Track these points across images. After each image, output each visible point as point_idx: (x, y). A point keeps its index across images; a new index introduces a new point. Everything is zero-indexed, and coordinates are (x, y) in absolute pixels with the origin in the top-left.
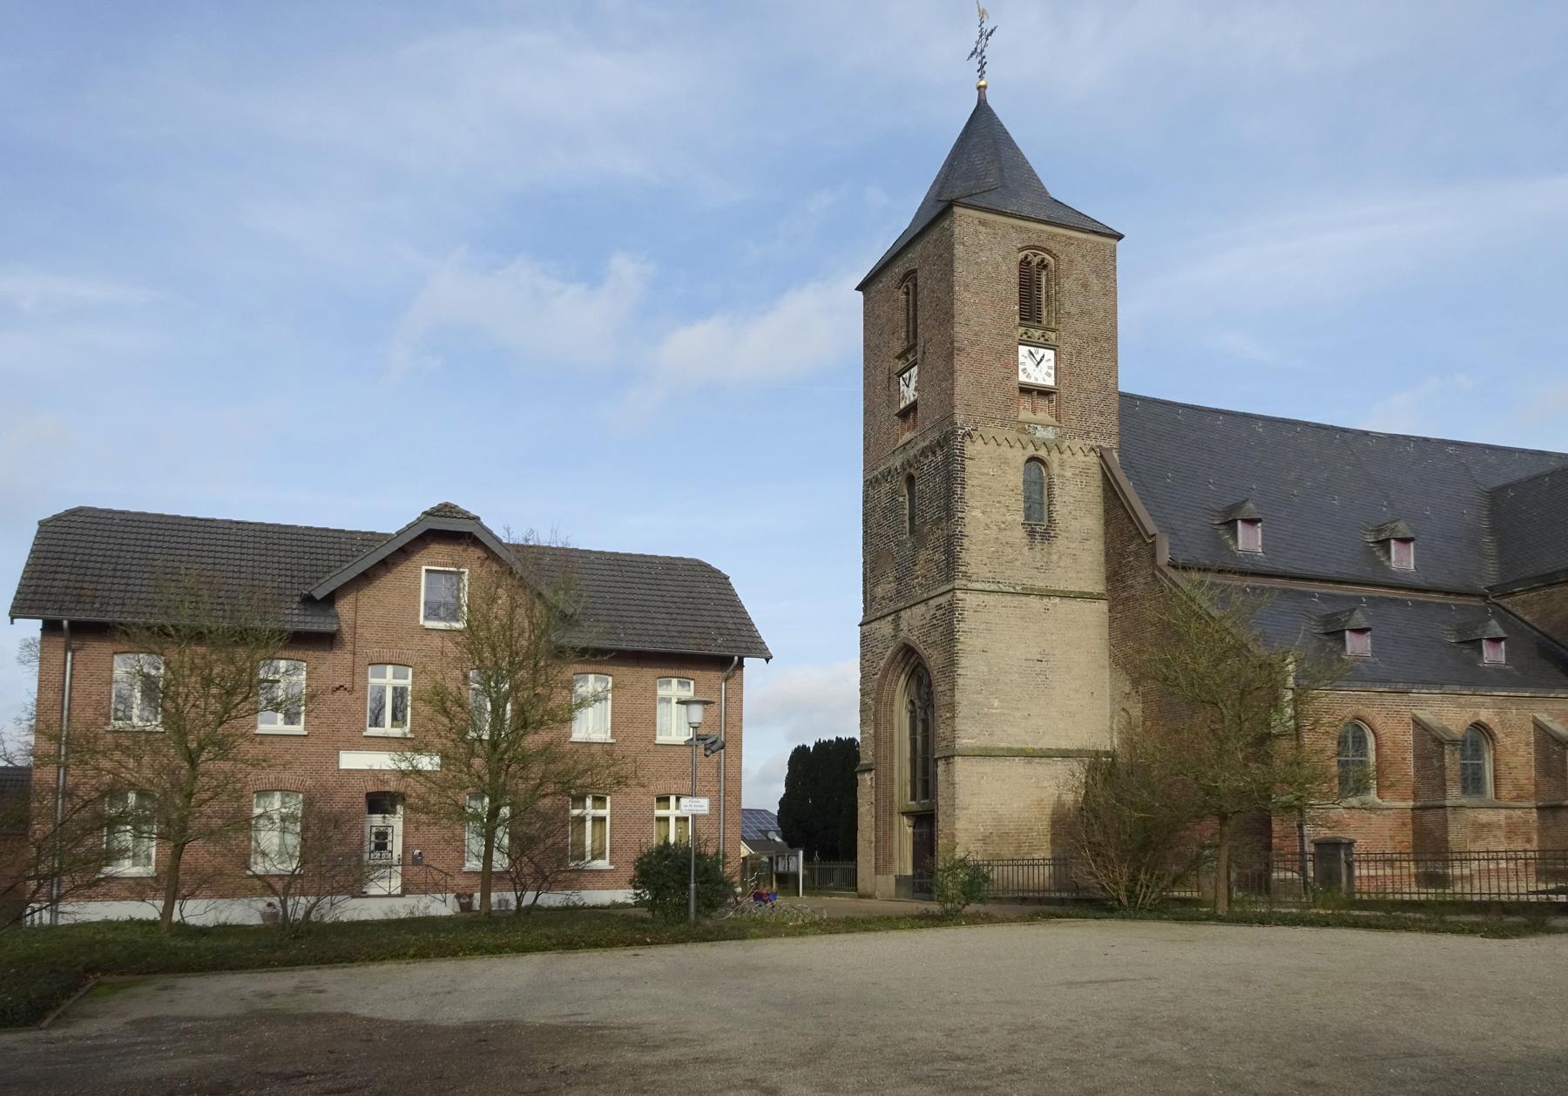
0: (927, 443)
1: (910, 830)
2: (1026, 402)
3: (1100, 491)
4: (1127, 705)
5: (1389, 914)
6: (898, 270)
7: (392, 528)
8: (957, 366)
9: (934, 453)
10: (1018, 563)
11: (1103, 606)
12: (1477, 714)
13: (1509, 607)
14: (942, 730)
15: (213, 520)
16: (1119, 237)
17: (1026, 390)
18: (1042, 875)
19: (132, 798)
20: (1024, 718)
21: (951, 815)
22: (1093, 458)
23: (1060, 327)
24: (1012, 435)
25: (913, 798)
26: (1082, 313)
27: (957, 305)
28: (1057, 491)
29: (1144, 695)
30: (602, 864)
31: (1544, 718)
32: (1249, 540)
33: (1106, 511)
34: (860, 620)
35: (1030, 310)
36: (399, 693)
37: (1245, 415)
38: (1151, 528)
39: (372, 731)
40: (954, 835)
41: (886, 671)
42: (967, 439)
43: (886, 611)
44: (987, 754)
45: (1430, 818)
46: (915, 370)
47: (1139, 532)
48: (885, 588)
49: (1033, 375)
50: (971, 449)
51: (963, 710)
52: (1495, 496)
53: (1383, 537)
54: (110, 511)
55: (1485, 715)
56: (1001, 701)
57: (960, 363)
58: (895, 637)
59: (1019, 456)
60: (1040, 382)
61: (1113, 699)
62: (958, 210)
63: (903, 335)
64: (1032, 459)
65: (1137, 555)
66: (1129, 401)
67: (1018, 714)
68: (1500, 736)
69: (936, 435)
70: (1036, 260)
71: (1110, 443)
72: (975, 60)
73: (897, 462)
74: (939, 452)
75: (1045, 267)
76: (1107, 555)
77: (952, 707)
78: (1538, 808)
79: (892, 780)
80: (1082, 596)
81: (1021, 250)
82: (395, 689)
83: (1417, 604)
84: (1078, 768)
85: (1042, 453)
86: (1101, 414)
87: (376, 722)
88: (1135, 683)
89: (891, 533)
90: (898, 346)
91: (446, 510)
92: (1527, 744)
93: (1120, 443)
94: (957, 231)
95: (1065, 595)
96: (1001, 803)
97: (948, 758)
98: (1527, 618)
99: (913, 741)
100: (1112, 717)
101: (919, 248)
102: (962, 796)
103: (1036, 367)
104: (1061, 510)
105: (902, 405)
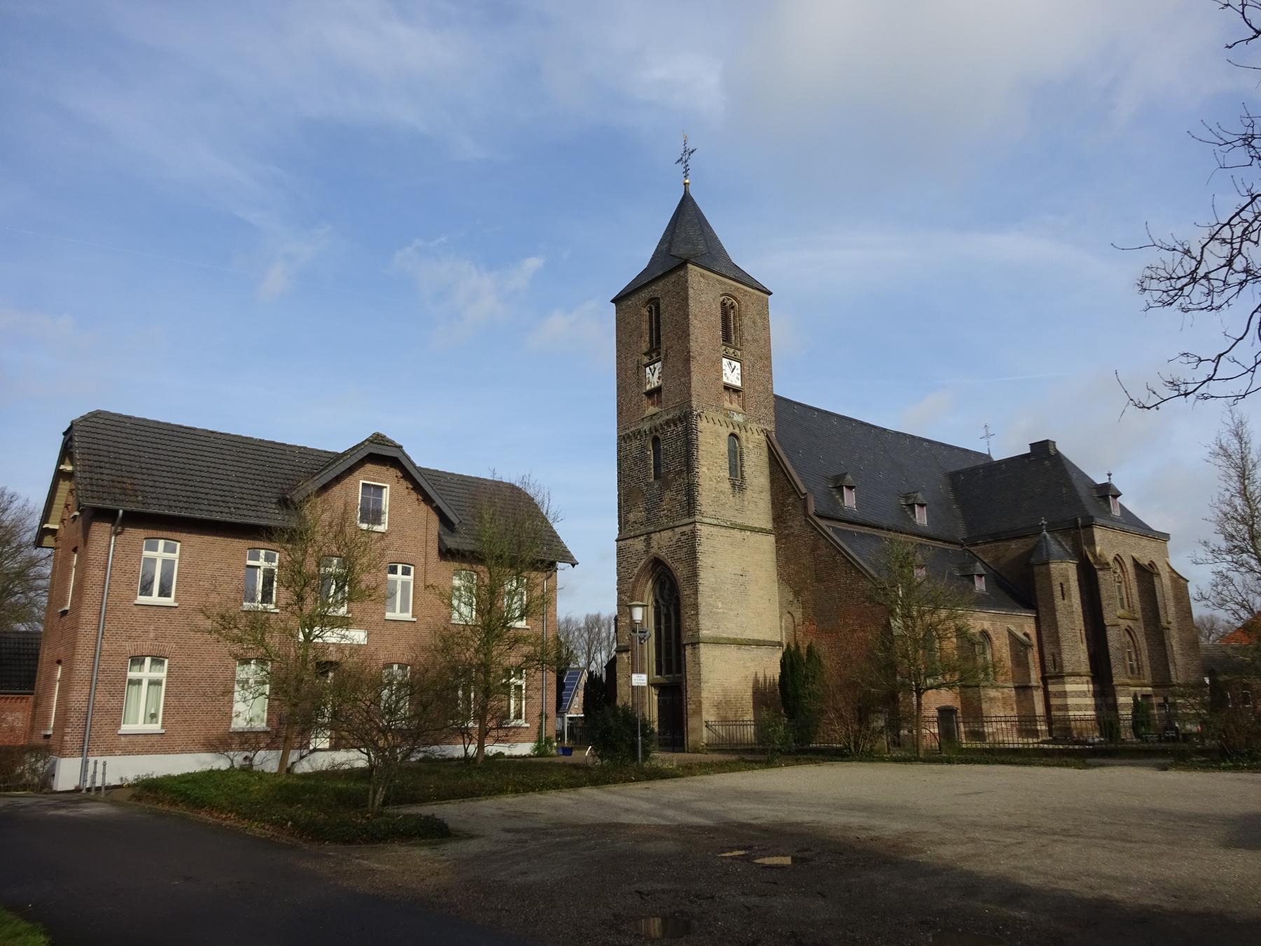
0: (670, 417)
1: (656, 698)
2: (726, 396)
4: (792, 609)
5: (932, 758)
6: (645, 295)
7: (339, 446)
9: (676, 425)
11: (772, 538)
14: (687, 623)
15: (195, 429)
16: (770, 293)
17: (727, 388)
19: (396, 667)
21: (698, 687)
22: (762, 437)
24: (722, 418)
25: (659, 673)
27: (691, 328)
30: (522, 722)
31: (1013, 628)
32: (849, 500)
35: (726, 338)
36: (168, 564)
38: (804, 491)
39: (142, 599)
40: (700, 703)
41: (638, 576)
43: (638, 532)
44: (717, 642)
45: (970, 692)
46: (658, 365)
47: (795, 491)
48: (636, 515)
50: (702, 425)
52: (953, 477)
53: (910, 502)
54: (121, 416)
55: (987, 625)
57: (694, 366)
58: (647, 552)
59: (725, 432)
61: (781, 604)
65: (794, 506)
67: (732, 613)
69: (678, 412)
72: (681, 167)
73: (646, 426)
76: (773, 503)
77: (696, 606)
80: (761, 531)
82: (164, 561)
83: (862, 535)
84: (778, 655)
85: (737, 431)
87: (146, 590)
89: (641, 476)
90: (645, 346)
91: (378, 439)
96: (729, 674)
97: (695, 644)
99: (658, 631)
100: (781, 617)
102: (705, 674)
103: (732, 374)
105: (648, 387)
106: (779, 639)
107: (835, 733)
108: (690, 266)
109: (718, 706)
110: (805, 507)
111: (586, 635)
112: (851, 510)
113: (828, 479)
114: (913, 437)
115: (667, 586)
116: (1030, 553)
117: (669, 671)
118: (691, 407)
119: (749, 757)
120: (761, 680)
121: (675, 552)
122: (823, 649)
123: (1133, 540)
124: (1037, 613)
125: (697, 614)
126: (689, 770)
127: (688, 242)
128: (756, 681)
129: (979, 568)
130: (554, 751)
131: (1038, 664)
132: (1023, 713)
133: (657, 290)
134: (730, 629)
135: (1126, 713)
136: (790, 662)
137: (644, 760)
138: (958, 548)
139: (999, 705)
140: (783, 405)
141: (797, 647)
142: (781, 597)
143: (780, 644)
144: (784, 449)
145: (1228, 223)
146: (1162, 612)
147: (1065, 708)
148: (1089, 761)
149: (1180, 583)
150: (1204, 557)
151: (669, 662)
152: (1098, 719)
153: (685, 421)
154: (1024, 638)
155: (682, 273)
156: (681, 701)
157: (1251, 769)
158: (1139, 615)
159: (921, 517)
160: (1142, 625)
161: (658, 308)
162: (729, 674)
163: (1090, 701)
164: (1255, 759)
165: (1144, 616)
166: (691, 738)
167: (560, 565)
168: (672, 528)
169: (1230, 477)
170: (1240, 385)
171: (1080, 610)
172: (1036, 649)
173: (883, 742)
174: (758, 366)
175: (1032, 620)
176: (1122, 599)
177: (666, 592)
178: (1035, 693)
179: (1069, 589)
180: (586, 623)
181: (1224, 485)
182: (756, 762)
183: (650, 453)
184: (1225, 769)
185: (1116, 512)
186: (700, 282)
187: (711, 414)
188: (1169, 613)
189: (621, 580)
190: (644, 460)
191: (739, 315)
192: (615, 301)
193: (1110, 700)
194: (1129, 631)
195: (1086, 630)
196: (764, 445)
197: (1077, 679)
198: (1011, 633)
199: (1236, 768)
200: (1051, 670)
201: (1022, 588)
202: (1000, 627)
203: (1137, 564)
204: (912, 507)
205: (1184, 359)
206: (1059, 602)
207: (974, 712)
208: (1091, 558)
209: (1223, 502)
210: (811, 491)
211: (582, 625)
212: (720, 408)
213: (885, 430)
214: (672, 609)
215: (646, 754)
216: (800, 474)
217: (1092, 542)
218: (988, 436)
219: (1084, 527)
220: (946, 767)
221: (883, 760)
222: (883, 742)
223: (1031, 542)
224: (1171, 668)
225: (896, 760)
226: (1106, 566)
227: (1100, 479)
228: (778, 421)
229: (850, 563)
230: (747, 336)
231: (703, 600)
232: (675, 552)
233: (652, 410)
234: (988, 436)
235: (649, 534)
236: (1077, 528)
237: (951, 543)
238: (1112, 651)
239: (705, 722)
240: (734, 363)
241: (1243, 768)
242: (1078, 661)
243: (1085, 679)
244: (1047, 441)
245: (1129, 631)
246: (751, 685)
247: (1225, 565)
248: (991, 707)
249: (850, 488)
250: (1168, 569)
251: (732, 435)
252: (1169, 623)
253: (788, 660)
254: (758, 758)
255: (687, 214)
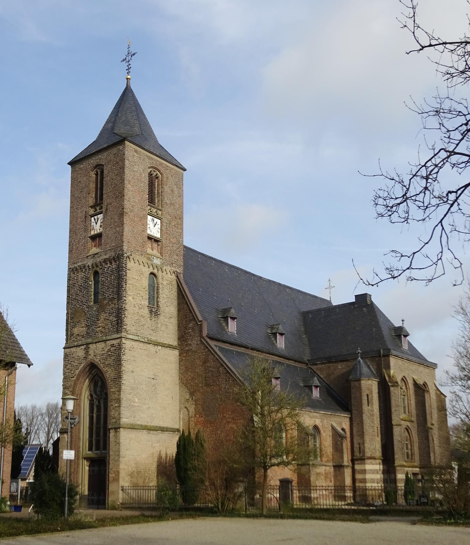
0: (107, 256)
1: (87, 468)
2: (149, 244)
3: (176, 294)
4: (188, 405)
6: (93, 161)
8: (125, 222)
9: (111, 263)
10: (146, 327)
11: (176, 352)
12: (315, 421)
13: (315, 370)
14: (112, 413)
17: (150, 238)
18: (152, 496)
20: (148, 409)
21: (117, 461)
22: (174, 277)
23: (163, 209)
24: (145, 260)
25: (90, 449)
27: (126, 190)
29: (196, 401)
31: (335, 425)
32: (232, 327)
33: (179, 304)
34: (64, 346)
35: (151, 200)
37: (221, 262)
38: (200, 319)
40: (118, 472)
41: (79, 375)
43: (80, 343)
44: (133, 427)
45: (304, 469)
46: (101, 216)
47: (194, 318)
48: (79, 330)
49: (153, 230)
50: (130, 264)
51: (124, 403)
52: (305, 315)
53: (274, 331)
55: (318, 422)
56: (139, 399)
57: (126, 220)
58: (85, 358)
59: (147, 271)
61: (180, 401)
64: (152, 273)
65: (193, 330)
67: (145, 407)
68: (322, 432)
69: (113, 254)
70: (155, 174)
71: (180, 270)
72: (125, 64)
73: (90, 262)
74: (113, 263)
75: (157, 178)
76: (179, 327)
77: (119, 400)
78: (334, 466)
79: (79, 439)
80: (170, 346)
81: (149, 168)
83: (239, 353)
84: (176, 438)
85: (155, 271)
86: (177, 255)
88: (192, 394)
89: (84, 300)
90: (91, 201)
92: (330, 436)
94: (126, 152)
95: (163, 345)
96: (140, 453)
97: (117, 429)
98: (321, 376)
100: (180, 411)
101: (105, 154)
103: (154, 228)
104: (162, 301)
105: (92, 233)
106: (177, 427)
107: (208, 496)
108: (126, 142)
109: (131, 475)
110: (201, 331)
111: (47, 419)
112: (232, 335)
113: (220, 313)
114: (280, 284)
115: (100, 384)
116: (349, 373)
117: (98, 448)
118: (122, 250)
119: (147, 513)
120: (164, 456)
121: (106, 359)
122: (205, 435)
123: (414, 367)
124: (351, 415)
125: (119, 406)
126: (102, 522)
127: (125, 127)
128: (160, 457)
129: (316, 381)
130: (8, 508)
131: (349, 450)
132: (338, 484)
133: (102, 158)
134: (143, 418)
135: (401, 485)
136: (184, 444)
137: (69, 515)
138: (304, 366)
139: (322, 477)
140: (191, 255)
141: (189, 433)
142: (181, 396)
143: (178, 430)
144: (189, 287)
145: (424, 166)
146: (428, 417)
147: (364, 481)
148: (371, 518)
149: (441, 397)
150: (446, 381)
151: (98, 442)
152: (385, 490)
153: (118, 260)
154: (341, 432)
155: (121, 147)
156: (105, 471)
157: (466, 524)
158: (414, 419)
159: (281, 343)
160: (416, 425)
161: (102, 172)
162: (140, 453)
163: (379, 476)
164: (468, 518)
165: (417, 420)
166: (111, 499)
167: (18, 365)
168: (105, 341)
169: (465, 328)
170: (428, 273)
171: (378, 413)
172: (349, 439)
173: (243, 501)
174: (174, 224)
175: (348, 420)
176: (404, 407)
177: (98, 389)
178: (346, 470)
179: (372, 398)
180: (48, 410)
181: (462, 334)
182: (152, 517)
183: (92, 283)
184: (450, 524)
185: (405, 347)
186: (134, 156)
187: (137, 257)
188: (433, 417)
189: (66, 379)
190: (87, 288)
191: (161, 184)
192: (71, 163)
193: (392, 476)
194: (407, 429)
195: (381, 428)
196: (175, 283)
197: (373, 461)
198: (333, 428)
199: (456, 524)
200: (357, 454)
201: (342, 398)
202: (326, 423)
203: (416, 384)
204: (275, 334)
205: (394, 254)
206: (365, 408)
207: (305, 483)
208: (387, 378)
209: (460, 345)
210: (206, 320)
211: (44, 411)
212: (143, 253)
213: (261, 278)
214: (102, 402)
215: (71, 510)
216: (198, 306)
217: (388, 367)
218: (330, 287)
219: (384, 356)
220: (280, 521)
221: (239, 516)
222: (243, 501)
223: (351, 364)
224: (432, 455)
225: (248, 516)
226: (395, 384)
227: (397, 324)
228: (186, 266)
229: (228, 372)
230: (166, 200)
231: (124, 396)
232: (106, 359)
233: (95, 250)
234: (330, 287)
235: (87, 344)
236: (380, 356)
237: (299, 362)
238: (396, 443)
239: (122, 486)
240: (156, 220)
241: (460, 524)
242: (375, 449)
243: (378, 461)
244: (366, 294)
245: (407, 429)
246: (156, 460)
247: (459, 388)
248: (317, 479)
249: (233, 319)
250: (435, 388)
251: (152, 273)
252: (432, 425)
253: (182, 442)
254: (154, 513)
255: (127, 102)
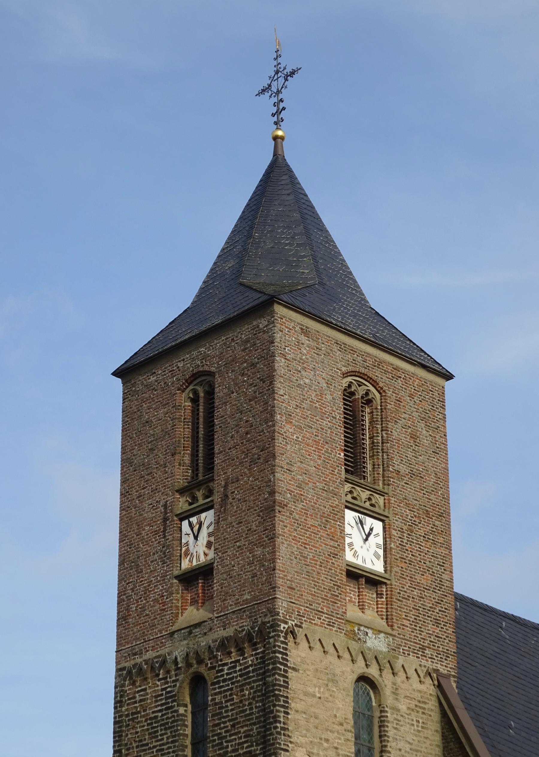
0: (230, 632)
2: (351, 591)
3: (437, 738)
6: (185, 363)
8: (279, 530)
9: (241, 651)
17: (354, 575)
22: (428, 688)
23: (389, 490)
24: (340, 640)
26: (412, 474)
27: (279, 441)
28: (391, 732)
42: (290, 637)
46: (208, 517)
50: (298, 653)
57: (283, 524)
59: (348, 672)
60: (368, 565)
62: (279, 310)
63: (187, 459)
64: (363, 679)
66: (467, 607)
69: (246, 624)
70: (361, 391)
71: (447, 667)
73: (178, 650)
74: (248, 651)
75: (369, 402)
81: (345, 375)
85: (373, 671)
86: (437, 623)
90: (181, 475)
93: (459, 667)
94: (278, 336)
101: (218, 342)
103: (364, 546)
105: (185, 564)
174: (424, 530)
